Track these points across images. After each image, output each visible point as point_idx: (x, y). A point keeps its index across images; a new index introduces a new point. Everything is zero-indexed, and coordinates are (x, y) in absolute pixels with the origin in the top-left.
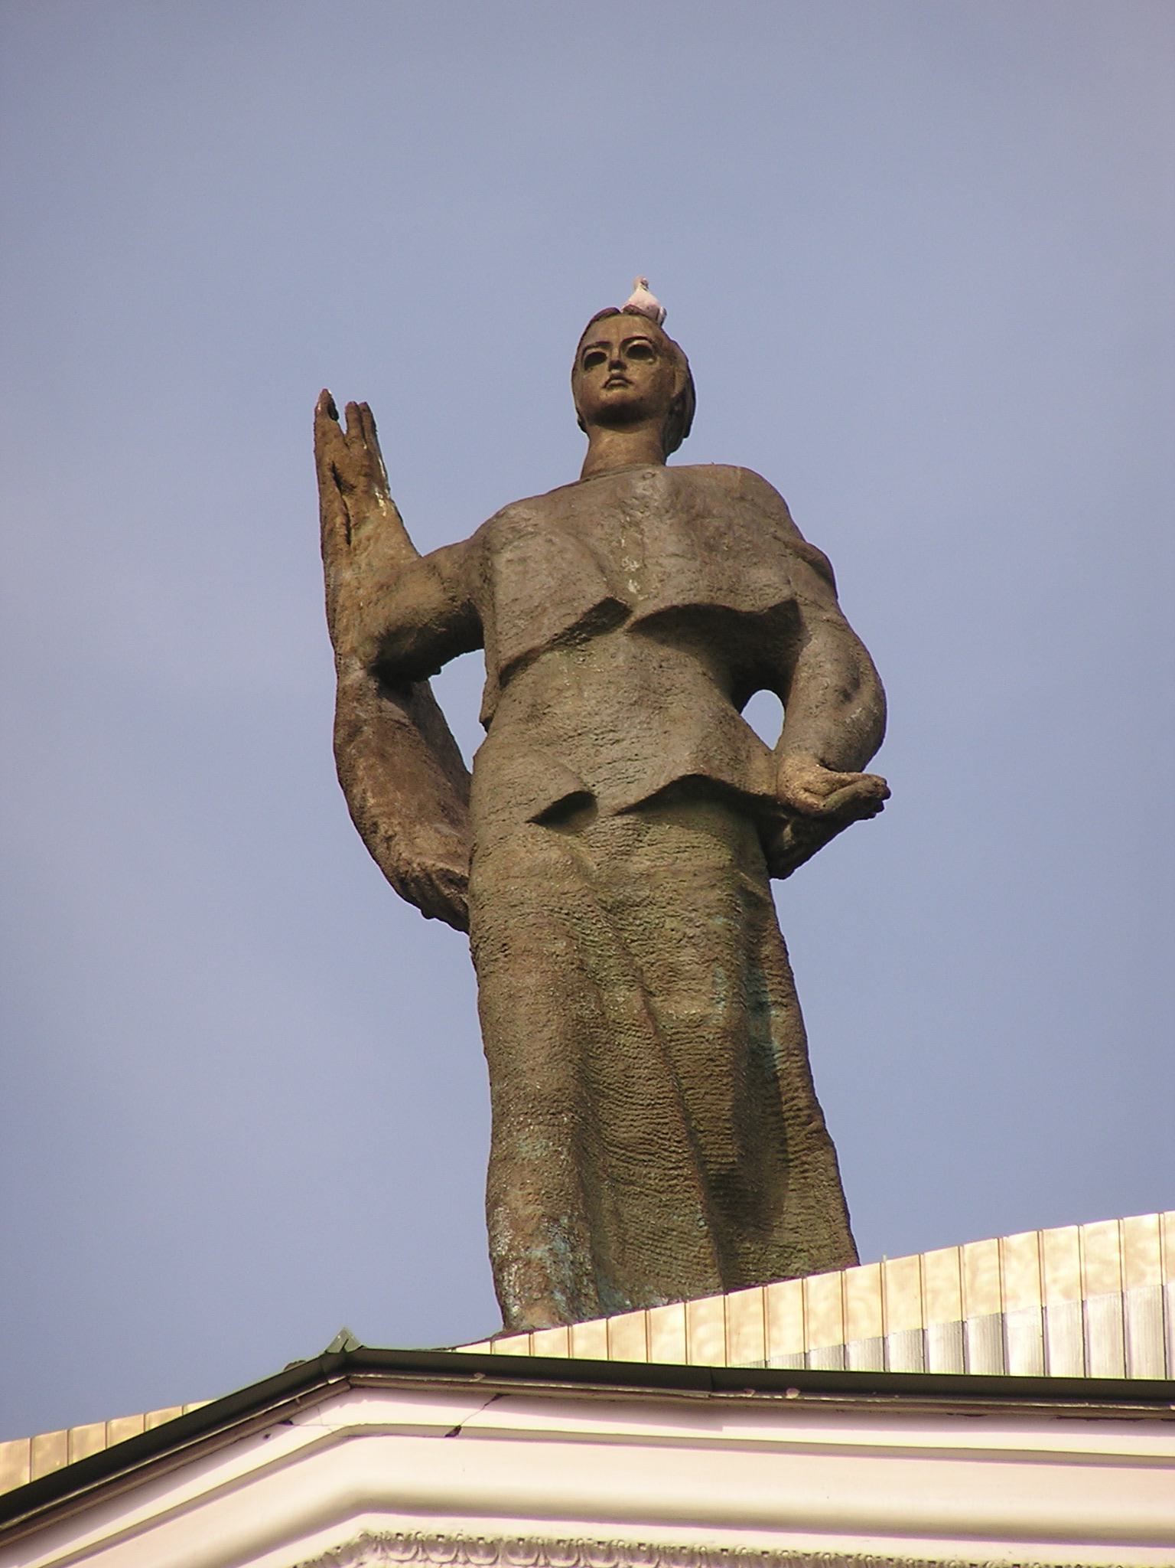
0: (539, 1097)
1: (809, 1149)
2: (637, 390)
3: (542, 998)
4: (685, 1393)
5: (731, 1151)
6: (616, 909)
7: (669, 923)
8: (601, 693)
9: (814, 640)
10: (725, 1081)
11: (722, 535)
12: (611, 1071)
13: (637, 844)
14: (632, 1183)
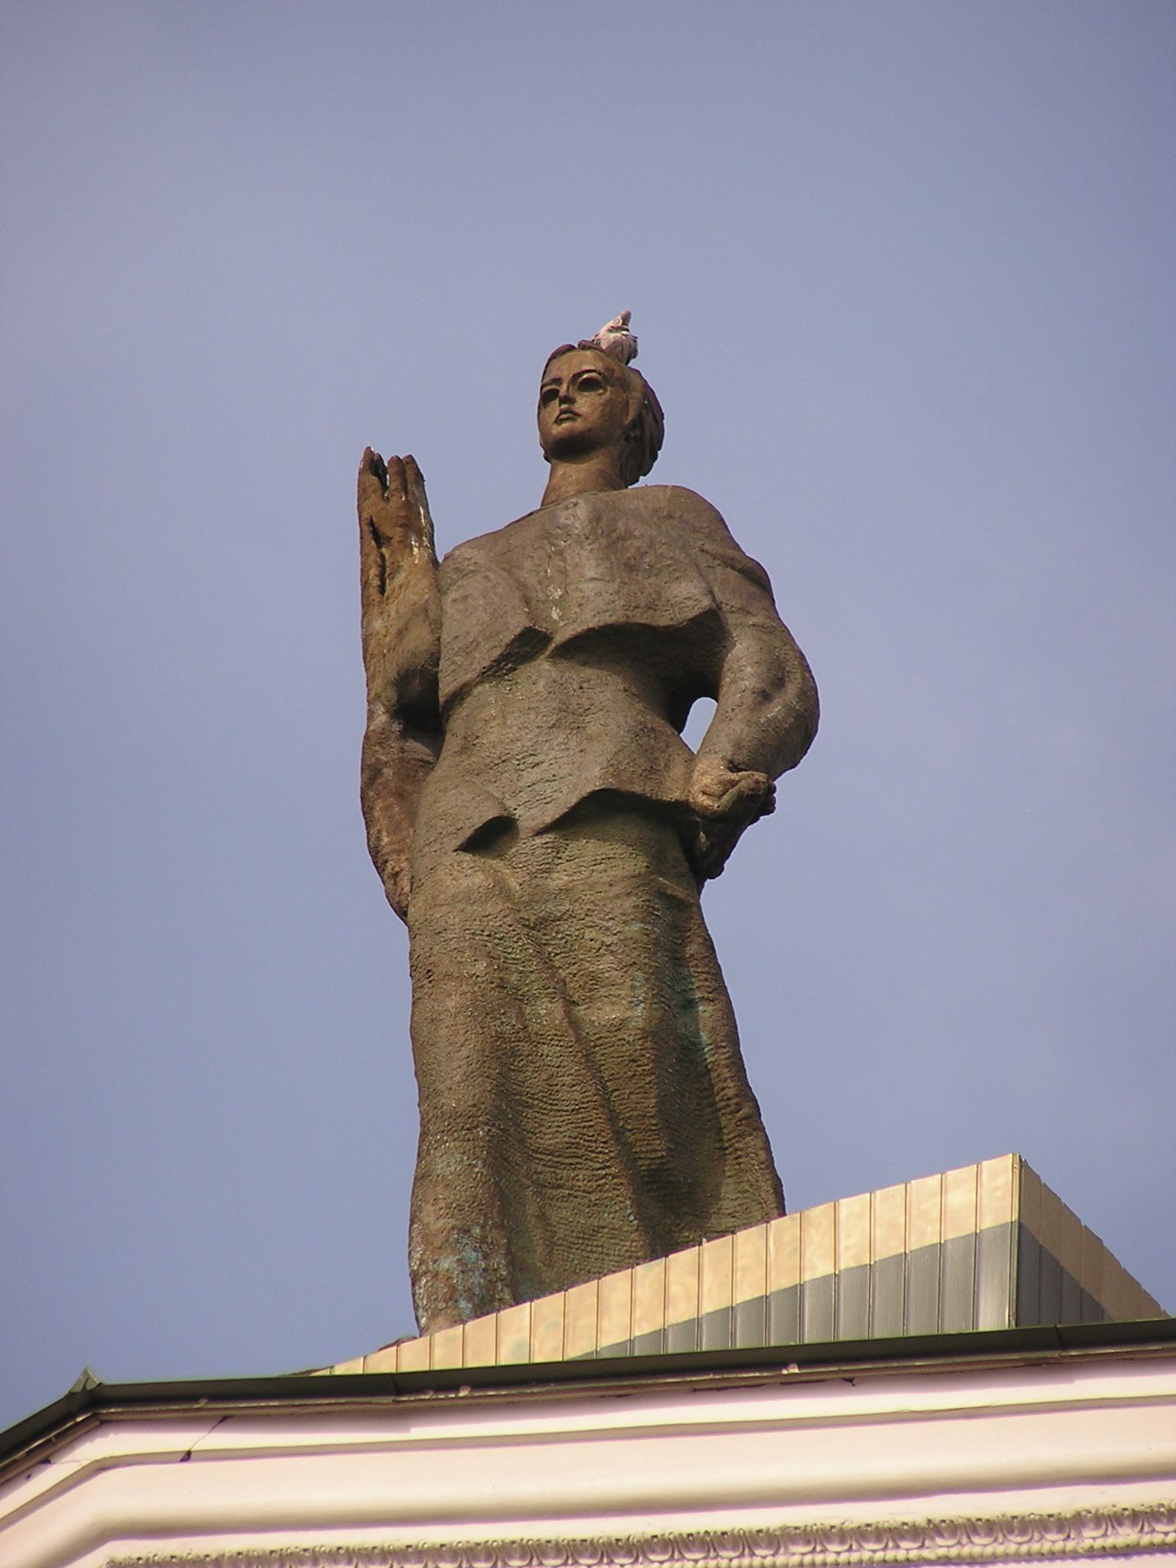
0: (454, 1115)
1: (740, 1135)
2: (605, 422)
3: (460, 1019)
4: (369, 1399)
5: (660, 1146)
6: (544, 923)
7: (589, 934)
8: (521, 720)
9: (738, 646)
10: (648, 1079)
11: (643, 555)
12: (534, 1081)
13: (557, 861)
14: (560, 1187)
